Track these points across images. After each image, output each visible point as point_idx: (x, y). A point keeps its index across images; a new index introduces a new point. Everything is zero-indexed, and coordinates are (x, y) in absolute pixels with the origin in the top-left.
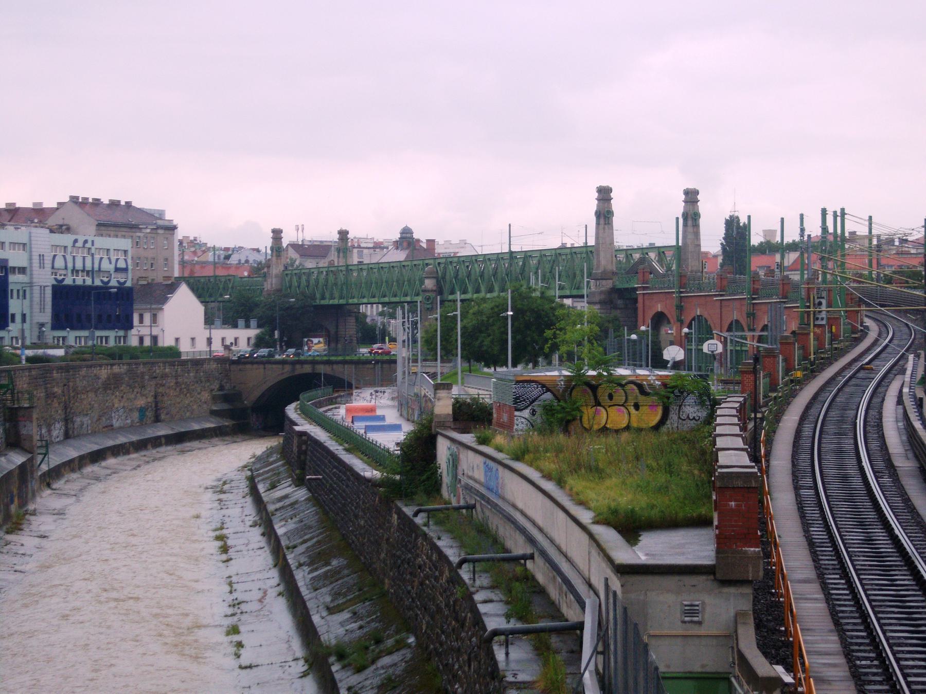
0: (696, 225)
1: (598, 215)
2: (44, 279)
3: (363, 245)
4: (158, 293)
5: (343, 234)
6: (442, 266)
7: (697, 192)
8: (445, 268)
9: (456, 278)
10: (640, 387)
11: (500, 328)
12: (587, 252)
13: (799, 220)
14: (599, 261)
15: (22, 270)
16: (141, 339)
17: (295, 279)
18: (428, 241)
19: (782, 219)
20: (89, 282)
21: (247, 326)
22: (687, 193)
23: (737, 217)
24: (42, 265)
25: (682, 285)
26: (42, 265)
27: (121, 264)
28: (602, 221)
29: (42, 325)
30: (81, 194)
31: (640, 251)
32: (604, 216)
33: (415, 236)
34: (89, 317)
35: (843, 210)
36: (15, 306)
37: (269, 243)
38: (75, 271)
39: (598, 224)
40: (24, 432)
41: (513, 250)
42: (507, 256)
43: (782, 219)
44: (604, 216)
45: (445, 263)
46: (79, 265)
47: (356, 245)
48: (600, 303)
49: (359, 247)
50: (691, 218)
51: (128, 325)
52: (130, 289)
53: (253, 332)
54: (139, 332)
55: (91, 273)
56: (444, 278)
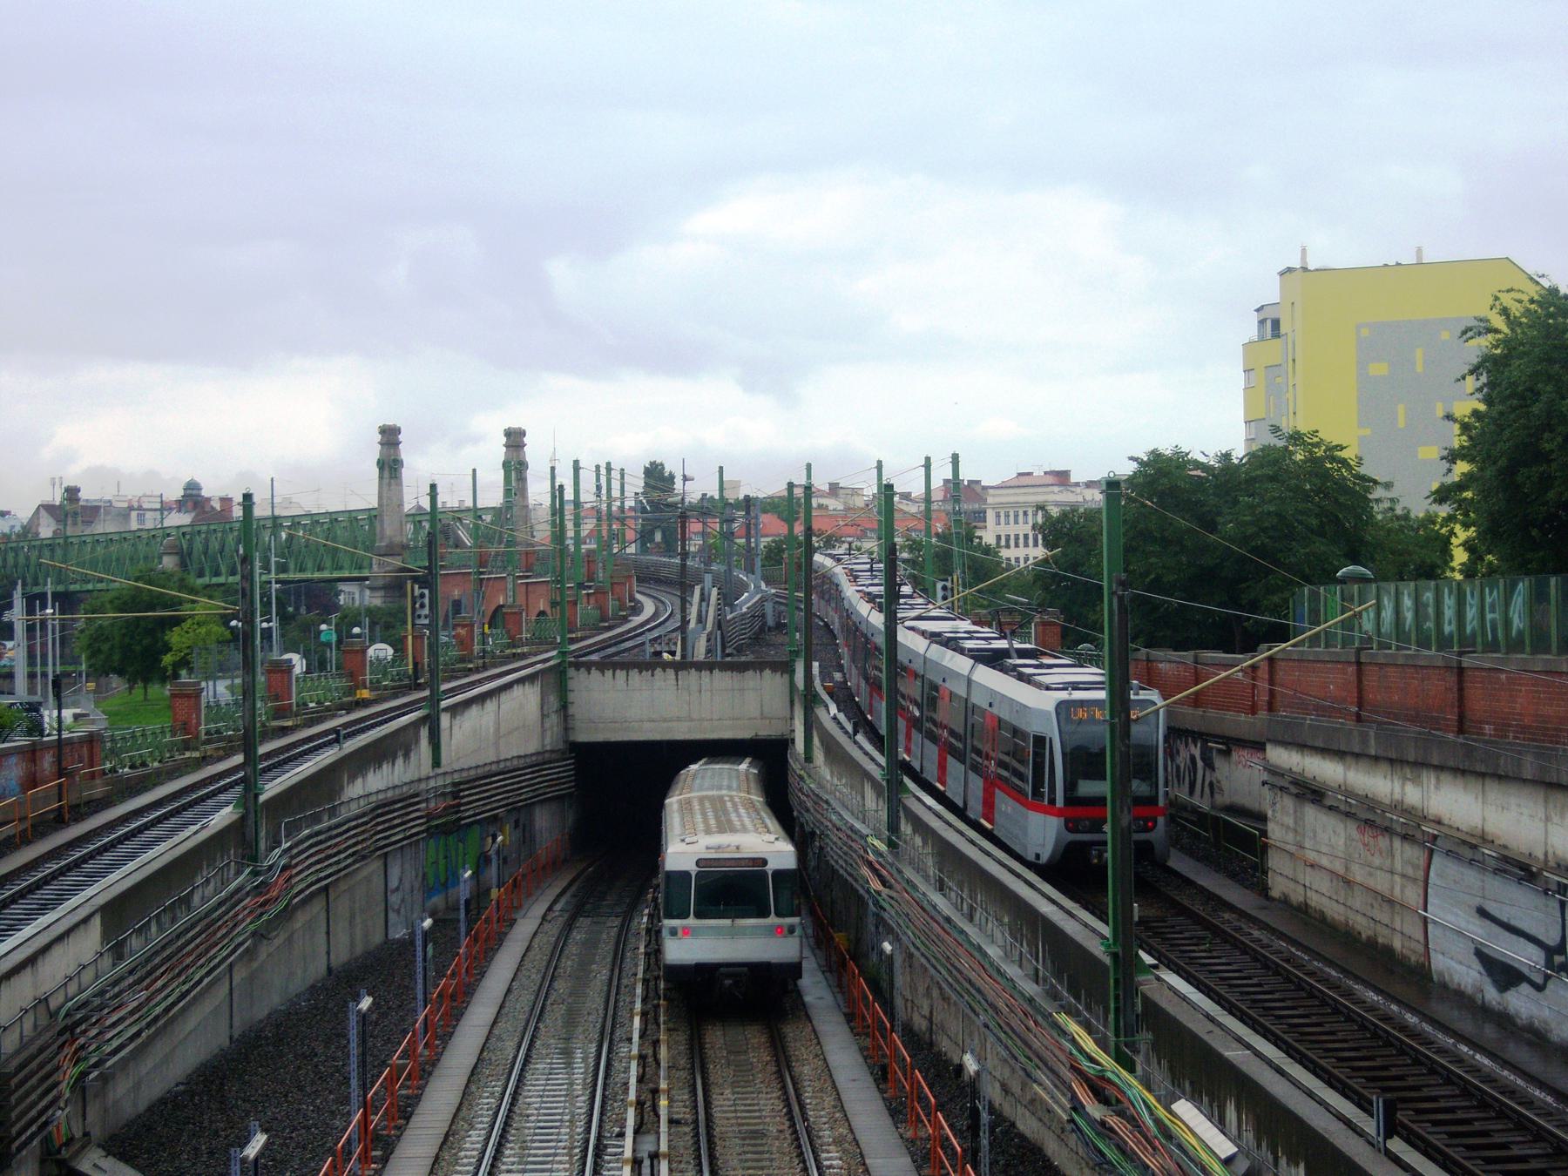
0: (522, 479)
1: (381, 464)
3: (145, 506)
5: (72, 493)
7: (523, 433)
8: (207, 540)
12: (373, 516)
14: (382, 529)
17: (11, 556)
19: (721, 468)
28: (386, 474)
32: (390, 467)
33: (205, 493)
35: (608, 464)
39: (381, 478)
41: (277, 513)
43: (721, 468)
44: (390, 467)
45: (208, 532)
48: (384, 588)
49: (140, 508)
50: (515, 468)
56: (190, 554)
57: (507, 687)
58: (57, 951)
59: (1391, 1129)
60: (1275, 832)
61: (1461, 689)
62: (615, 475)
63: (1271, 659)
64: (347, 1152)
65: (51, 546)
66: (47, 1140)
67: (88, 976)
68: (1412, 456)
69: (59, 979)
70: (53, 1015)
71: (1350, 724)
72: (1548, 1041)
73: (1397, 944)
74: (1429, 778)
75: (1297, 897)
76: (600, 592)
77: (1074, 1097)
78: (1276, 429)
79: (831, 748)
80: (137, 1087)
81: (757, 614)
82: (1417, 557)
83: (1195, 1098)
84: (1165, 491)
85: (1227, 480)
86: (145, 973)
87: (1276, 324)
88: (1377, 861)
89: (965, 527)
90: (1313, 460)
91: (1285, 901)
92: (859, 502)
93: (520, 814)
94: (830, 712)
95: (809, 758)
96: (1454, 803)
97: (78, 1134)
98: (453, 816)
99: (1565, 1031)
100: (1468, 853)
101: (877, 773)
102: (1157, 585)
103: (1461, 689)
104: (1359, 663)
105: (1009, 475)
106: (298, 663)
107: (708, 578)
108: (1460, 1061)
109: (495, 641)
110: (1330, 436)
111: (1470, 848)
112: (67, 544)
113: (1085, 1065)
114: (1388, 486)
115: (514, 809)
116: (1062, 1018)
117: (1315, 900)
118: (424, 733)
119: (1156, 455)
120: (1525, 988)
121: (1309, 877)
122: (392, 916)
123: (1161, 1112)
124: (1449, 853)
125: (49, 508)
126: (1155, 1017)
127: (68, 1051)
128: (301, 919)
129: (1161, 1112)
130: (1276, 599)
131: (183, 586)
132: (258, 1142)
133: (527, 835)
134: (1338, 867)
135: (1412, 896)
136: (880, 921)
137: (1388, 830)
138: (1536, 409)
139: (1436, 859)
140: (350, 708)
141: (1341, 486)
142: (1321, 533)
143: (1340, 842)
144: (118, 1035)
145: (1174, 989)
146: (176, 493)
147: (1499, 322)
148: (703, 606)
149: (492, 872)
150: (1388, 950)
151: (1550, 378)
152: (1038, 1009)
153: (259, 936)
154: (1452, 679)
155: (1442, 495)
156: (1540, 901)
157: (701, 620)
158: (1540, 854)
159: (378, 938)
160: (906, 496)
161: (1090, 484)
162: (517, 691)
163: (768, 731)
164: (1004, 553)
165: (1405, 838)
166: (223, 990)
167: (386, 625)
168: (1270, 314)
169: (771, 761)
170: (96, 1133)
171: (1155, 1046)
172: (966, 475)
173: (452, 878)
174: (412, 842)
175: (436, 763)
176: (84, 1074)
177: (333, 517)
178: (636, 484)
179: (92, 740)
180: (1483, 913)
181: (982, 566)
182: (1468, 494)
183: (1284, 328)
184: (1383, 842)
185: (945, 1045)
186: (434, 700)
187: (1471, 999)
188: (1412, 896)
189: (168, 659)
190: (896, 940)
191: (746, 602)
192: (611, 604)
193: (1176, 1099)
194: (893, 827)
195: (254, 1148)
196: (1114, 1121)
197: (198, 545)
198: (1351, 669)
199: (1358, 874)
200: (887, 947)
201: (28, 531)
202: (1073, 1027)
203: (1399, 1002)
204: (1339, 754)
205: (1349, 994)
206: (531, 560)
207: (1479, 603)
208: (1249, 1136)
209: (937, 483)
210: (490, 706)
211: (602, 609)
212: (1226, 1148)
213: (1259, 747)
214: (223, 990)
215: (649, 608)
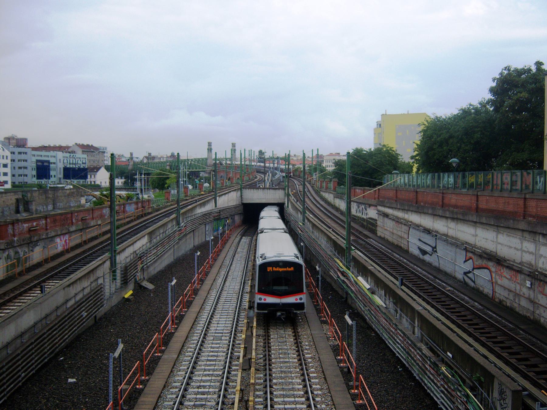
2: (61, 166)
4: (98, 169)
5: (150, 154)
10: (120, 197)
12: (206, 159)
15: (54, 163)
16: (91, 182)
18: (480, 104)
20: (74, 166)
21: (122, 178)
22: (208, 143)
24: (60, 162)
26: (60, 162)
27: (84, 162)
29: (60, 179)
30: (78, 143)
32: (210, 150)
36: (52, 173)
37: (129, 156)
38: (70, 164)
40: (30, 208)
44: (210, 150)
46: (71, 162)
50: (234, 151)
51: (85, 177)
52: (86, 169)
53: (123, 180)
54: (90, 179)
55: (75, 164)
57: (230, 192)
58: (138, 242)
59: (402, 284)
60: (379, 223)
61: (417, 196)
62: (252, 152)
63: (379, 189)
64: (194, 282)
65: (146, 164)
66: (136, 279)
67: (144, 247)
68: (407, 150)
69: (138, 248)
70: (137, 255)
71: (394, 202)
72: (483, 294)
73: (402, 246)
74: (410, 213)
75: (383, 236)
76: (249, 174)
77: (338, 275)
78: (380, 144)
79: (293, 205)
80: (155, 269)
81: (279, 179)
82: (406, 169)
83: (362, 276)
84: (358, 158)
85: (371, 154)
86: (156, 246)
87: (380, 125)
88: (399, 229)
89: (320, 164)
90: (387, 150)
91: (380, 237)
92: (299, 158)
93: (232, 216)
94: (292, 198)
95: (288, 207)
96: (415, 218)
97: (142, 278)
98: (218, 217)
99: (546, 317)
100: (417, 228)
101: (301, 210)
102: (356, 174)
103: (417, 196)
104: (396, 190)
105: (328, 154)
106: (190, 187)
107: (270, 172)
108: (414, 269)
109: (229, 183)
110: (391, 146)
111: (417, 227)
112: (149, 163)
113: (340, 269)
114: (401, 156)
115: (231, 215)
116: (336, 259)
117: (386, 237)
118: (213, 200)
119: (357, 149)
120: (428, 255)
121: (385, 232)
122: (207, 236)
123: (355, 279)
124: (413, 228)
125: (146, 157)
126: (355, 260)
127: (140, 262)
128: (188, 236)
129: (355, 279)
130: (380, 177)
131: (169, 172)
132: (175, 281)
133: (233, 219)
134: (391, 230)
135: (406, 236)
136: (301, 239)
137: (401, 223)
138: (432, 140)
139: (411, 229)
140: (199, 196)
141: (393, 155)
142: (389, 164)
143: (392, 225)
144: (150, 259)
145: (358, 254)
146: (169, 155)
147: (426, 123)
148: (268, 178)
149: (226, 228)
150: (401, 247)
151: (435, 134)
152: (331, 257)
153: (179, 239)
154: (415, 194)
155: (412, 158)
156: (432, 238)
157: (268, 180)
158: (432, 229)
159: (204, 240)
160: (308, 157)
161: (344, 156)
162: (232, 193)
163: (280, 201)
164: (327, 168)
165: (405, 225)
166: (172, 250)
167: (208, 180)
168: (379, 123)
169: (281, 207)
170: (146, 278)
171: (354, 266)
172: (320, 153)
173: (218, 230)
174: (211, 222)
175: (216, 206)
176: (143, 266)
177: (199, 159)
178: (257, 154)
179: (149, 201)
180: (420, 240)
181: (322, 170)
182: (417, 158)
183: (382, 126)
184: (400, 225)
185: (313, 263)
186: (216, 194)
187: (417, 257)
188: (406, 236)
189: (166, 186)
190: (304, 242)
191: (277, 177)
192: (251, 177)
193: (358, 276)
194: (304, 220)
195: (173, 283)
196: (345, 280)
197: (173, 164)
198: (395, 191)
199: (395, 232)
200: (302, 244)
201: (142, 161)
202: (338, 261)
203: (403, 257)
204: (392, 208)
205: (393, 255)
206: (237, 167)
207: (416, 178)
208: (373, 284)
209: (314, 155)
210: (227, 195)
211: (249, 177)
212: (368, 287)
213: (376, 206)
214: (172, 250)
215: (258, 177)
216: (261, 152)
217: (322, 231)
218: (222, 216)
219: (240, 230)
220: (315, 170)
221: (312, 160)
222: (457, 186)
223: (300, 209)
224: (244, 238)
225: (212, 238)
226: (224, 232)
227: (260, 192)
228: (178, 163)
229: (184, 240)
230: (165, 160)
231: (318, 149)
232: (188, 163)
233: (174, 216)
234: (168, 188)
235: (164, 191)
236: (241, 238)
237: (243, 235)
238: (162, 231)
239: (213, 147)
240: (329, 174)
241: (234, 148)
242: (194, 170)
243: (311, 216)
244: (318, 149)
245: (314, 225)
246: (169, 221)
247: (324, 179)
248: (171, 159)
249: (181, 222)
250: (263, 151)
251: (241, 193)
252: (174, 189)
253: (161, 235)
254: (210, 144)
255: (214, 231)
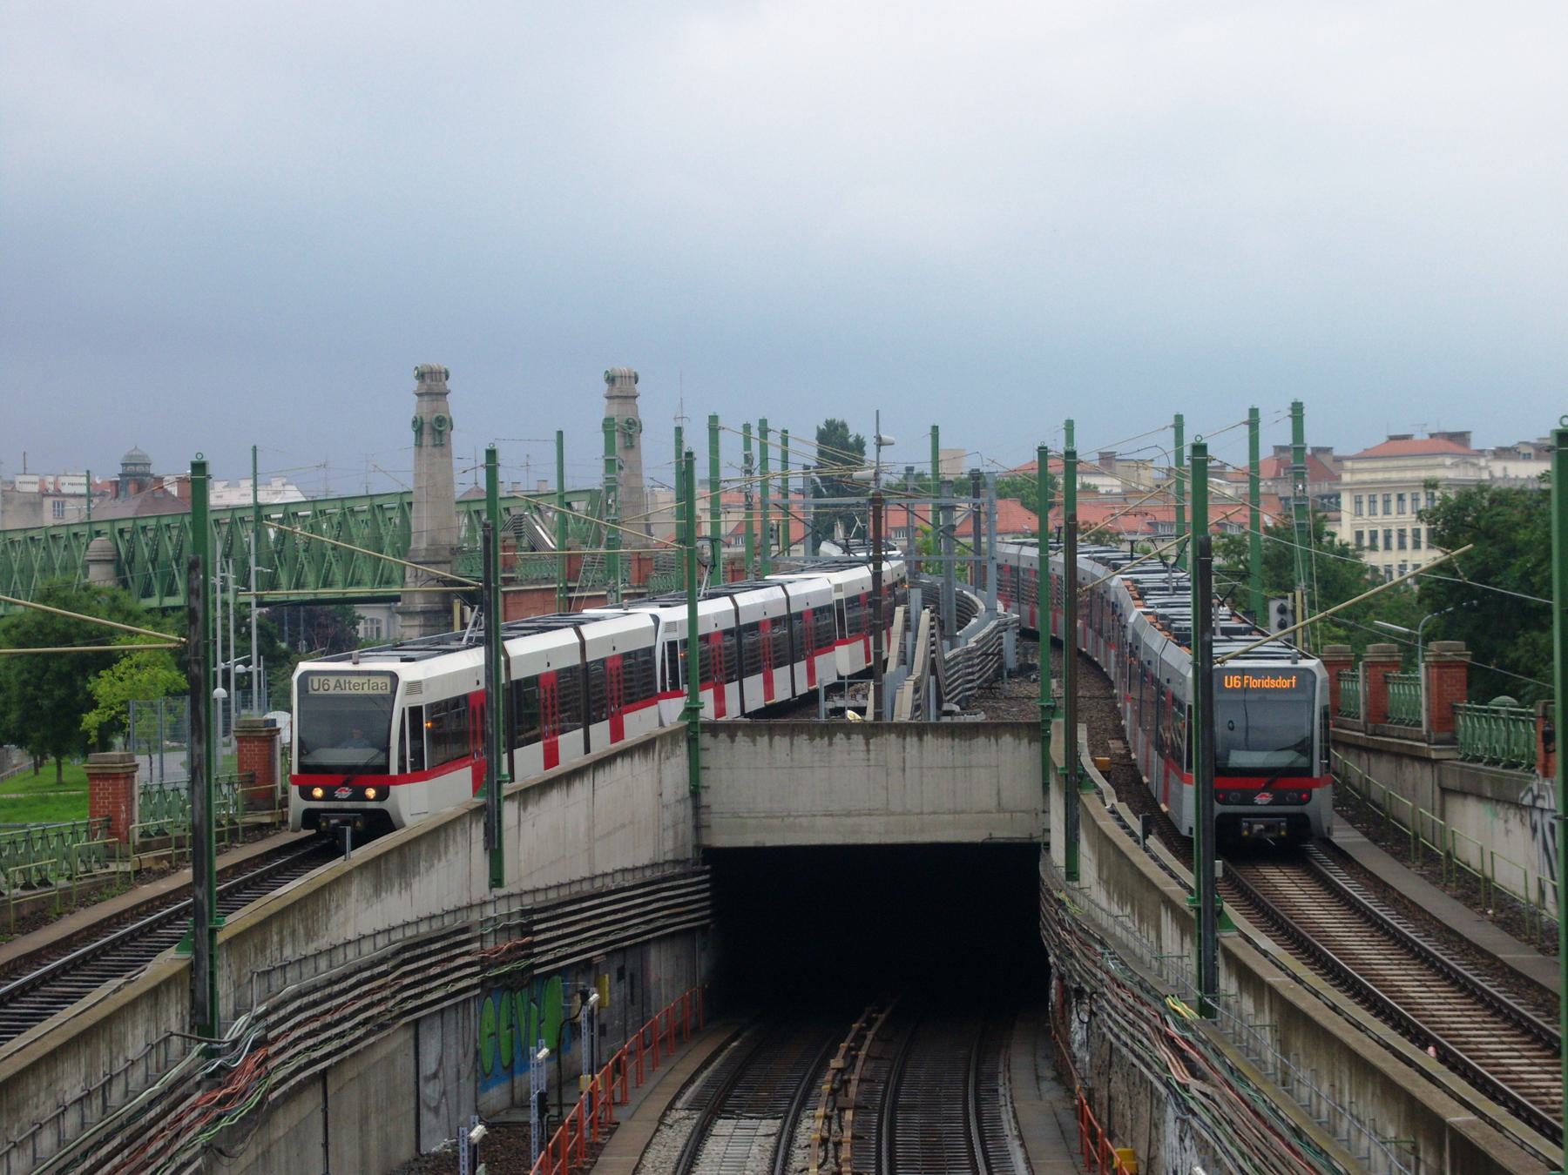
6: (127, 536)
9: (154, 561)
11: (20, 673)
12: (406, 505)
13: (929, 439)
18: (858, 437)
19: (935, 429)
23: (844, 426)
25: (572, 575)
31: (587, 497)
32: (433, 431)
34: (645, 662)
35: (763, 422)
42: (250, 515)
44: (433, 431)
47: (51, 488)
50: (622, 433)
62: (774, 439)
81: (990, 650)
89: (1311, 521)
93: (626, 959)
94: (1104, 805)
95: (1072, 873)
98: (518, 965)
101: (1184, 900)
115: (617, 951)
118: (478, 832)
122: (427, 1118)
128: (283, 1123)
131: (115, 609)
149: (582, 1050)
157: (905, 660)
159: (405, 1153)
172: (1311, 440)
173: (515, 1065)
174: (460, 1004)
175: (496, 880)
178: (806, 452)
181: (1338, 577)
189: (91, 720)
191: (974, 634)
194: (1208, 984)
216: (834, 439)
217: (1363, 1068)
218: (544, 957)
219: (690, 1067)
220: (1279, 569)
221: (1254, 495)
222: (945, 492)
223: (1172, 889)
224: (723, 1127)
225: (478, 1131)
226: (563, 1079)
227: (847, 753)
228: (201, 543)
229: (248, 1154)
230: (74, 513)
231: (1297, 410)
232: (260, 535)
233: (169, 961)
234: (105, 745)
235: (75, 768)
236: (701, 1135)
237: (715, 1107)
238: (71, 1084)
239: (457, 406)
240: (1392, 603)
241: (619, 412)
242: (307, 593)
243: (1266, 943)
244: (1297, 410)
245: (1291, 1018)
246: (133, 1004)
247: (1360, 645)
248: (124, 509)
249: (225, 1007)
250: (859, 427)
251: (695, 769)
252: (153, 747)
253: (71, 1121)
254: (432, 383)
255: (483, 1079)
